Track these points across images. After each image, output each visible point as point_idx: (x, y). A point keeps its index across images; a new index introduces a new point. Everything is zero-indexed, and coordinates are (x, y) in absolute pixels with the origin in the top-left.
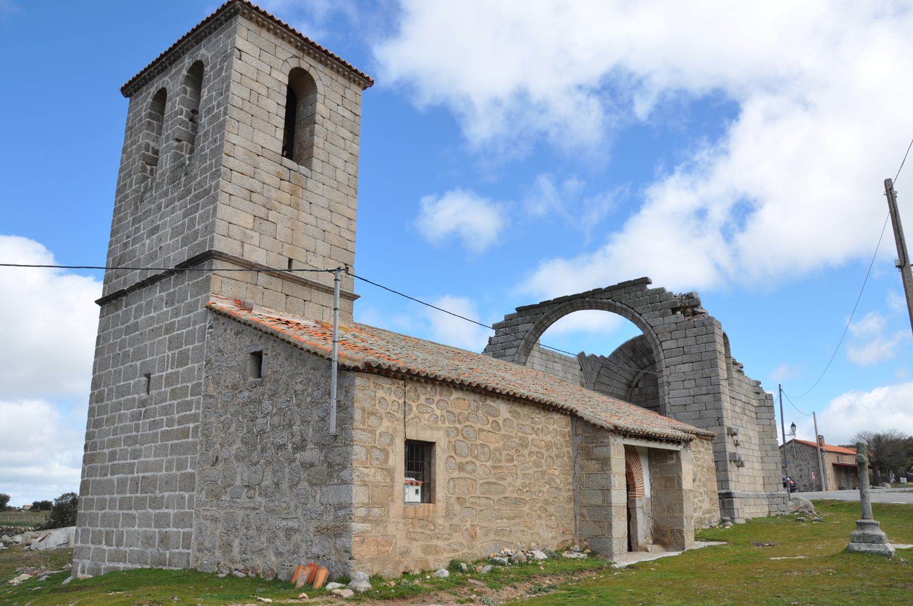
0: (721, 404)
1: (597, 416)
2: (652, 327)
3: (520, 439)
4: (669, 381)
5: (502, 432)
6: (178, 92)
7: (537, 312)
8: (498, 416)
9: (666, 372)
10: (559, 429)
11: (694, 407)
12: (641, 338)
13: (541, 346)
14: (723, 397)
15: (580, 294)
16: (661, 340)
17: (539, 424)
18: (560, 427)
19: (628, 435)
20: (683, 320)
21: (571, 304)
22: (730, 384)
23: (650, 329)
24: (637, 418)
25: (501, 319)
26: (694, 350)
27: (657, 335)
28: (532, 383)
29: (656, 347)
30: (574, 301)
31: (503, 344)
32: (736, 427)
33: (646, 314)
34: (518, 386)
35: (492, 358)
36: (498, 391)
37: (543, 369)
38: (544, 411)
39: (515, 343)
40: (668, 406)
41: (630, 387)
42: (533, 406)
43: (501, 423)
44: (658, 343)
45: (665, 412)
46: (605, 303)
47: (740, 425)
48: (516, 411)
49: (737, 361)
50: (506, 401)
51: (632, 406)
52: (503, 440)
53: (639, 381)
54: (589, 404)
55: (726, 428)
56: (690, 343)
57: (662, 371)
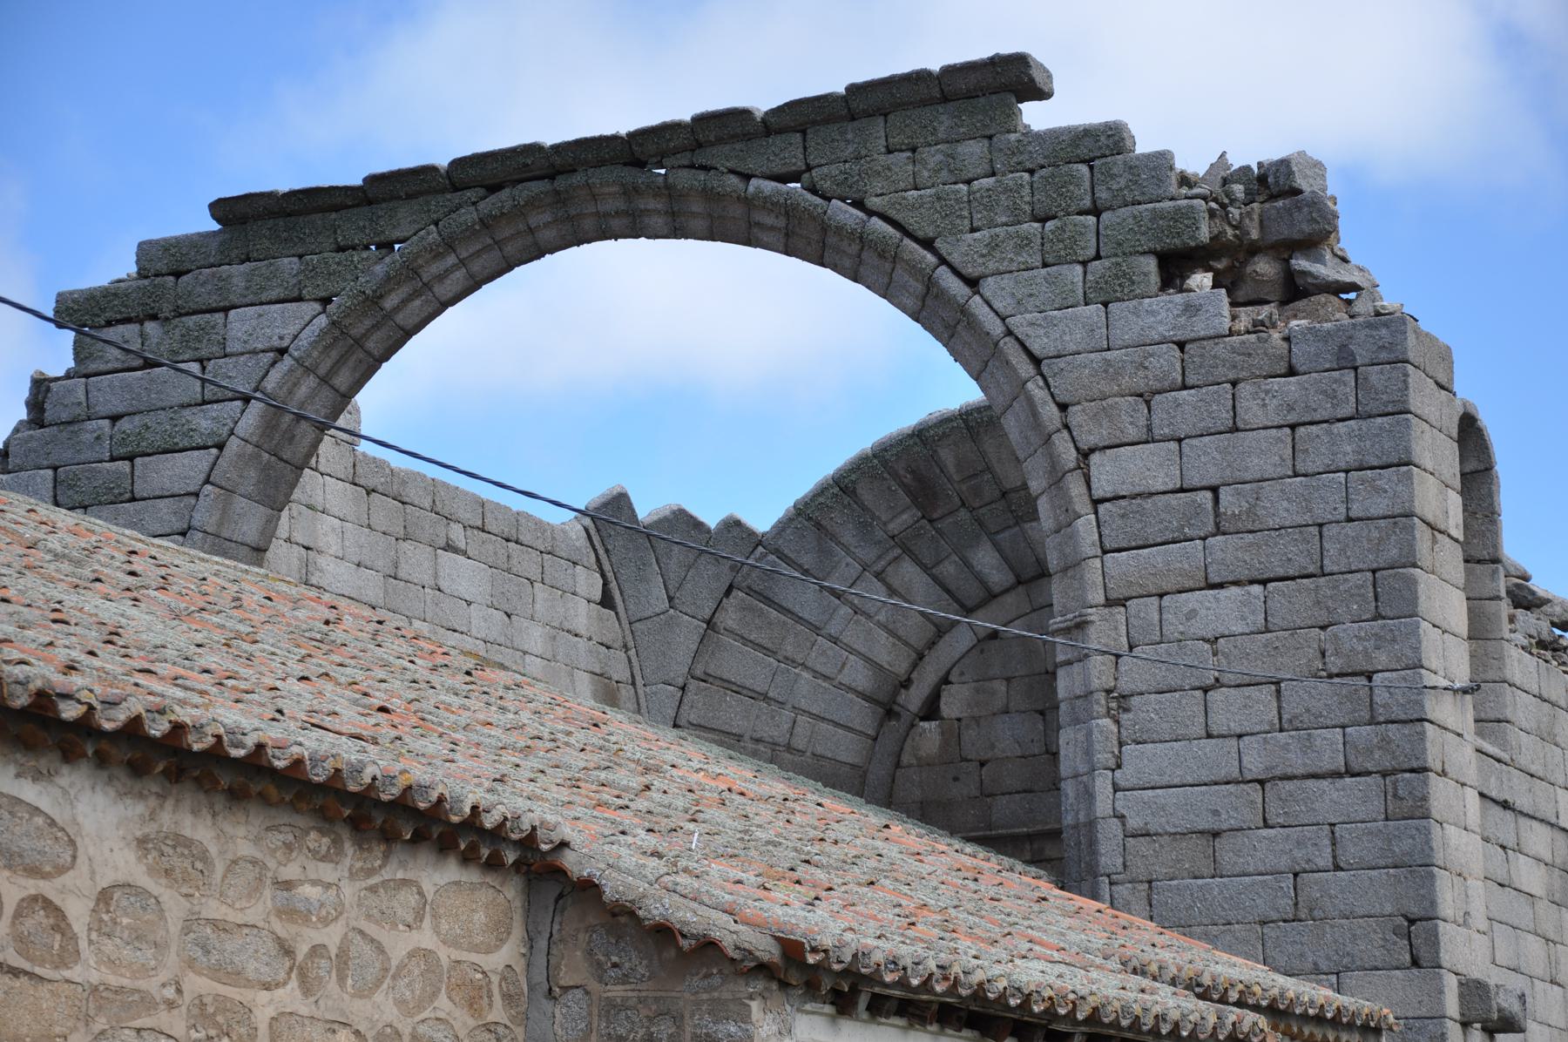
0: (1427, 832)
1: (682, 879)
2: (1036, 361)
3: (201, 1012)
4: (1125, 685)
5: (87, 971)
6: (647, 872)
7: (349, 234)
8: (61, 870)
9: (1105, 630)
10: (445, 955)
11: (1266, 849)
12: (969, 424)
13: (364, 447)
14: (1440, 793)
15: (615, 138)
16: (1086, 441)
17: (326, 921)
18: (453, 943)
19: (863, 1002)
20: (1227, 323)
21: (560, 199)
22: (1488, 723)
23: (1025, 368)
24: (922, 895)
25: (114, 265)
26: (1280, 506)
27: (1063, 407)
28: (299, 670)
29: (1057, 480)
30: (577, 179)
31: (124, 424)
32: (1516, 983)
33: (1006, 281)
34: (205, 682)
35: (46, 511)
36: (69, 711)
37: (371, 586)
38: (359, 844)
39: (204, 422)
40: (1109, 838)
41: (889, 712)
42: (293, 807)
43: (78, 912)
44: (1069, 456)
45: (1093, 871)
46: (768, 204)
47: (1539, 969)
48: (181, 842)
49: (1540, 584)
50: (121, 773)
51: (896, 829)
52: (88, 1020)
53: (946, 680)
54: (641, 804)
55: (1451, 982)
56: (1256, 465)
57: (1081, 625)
